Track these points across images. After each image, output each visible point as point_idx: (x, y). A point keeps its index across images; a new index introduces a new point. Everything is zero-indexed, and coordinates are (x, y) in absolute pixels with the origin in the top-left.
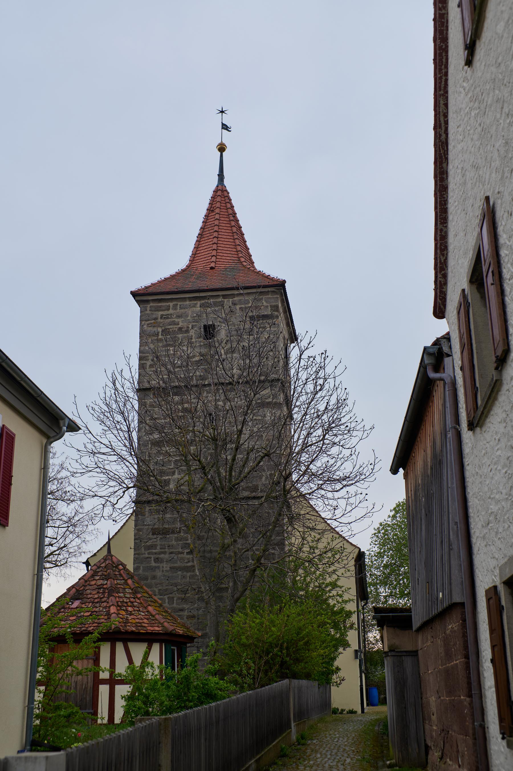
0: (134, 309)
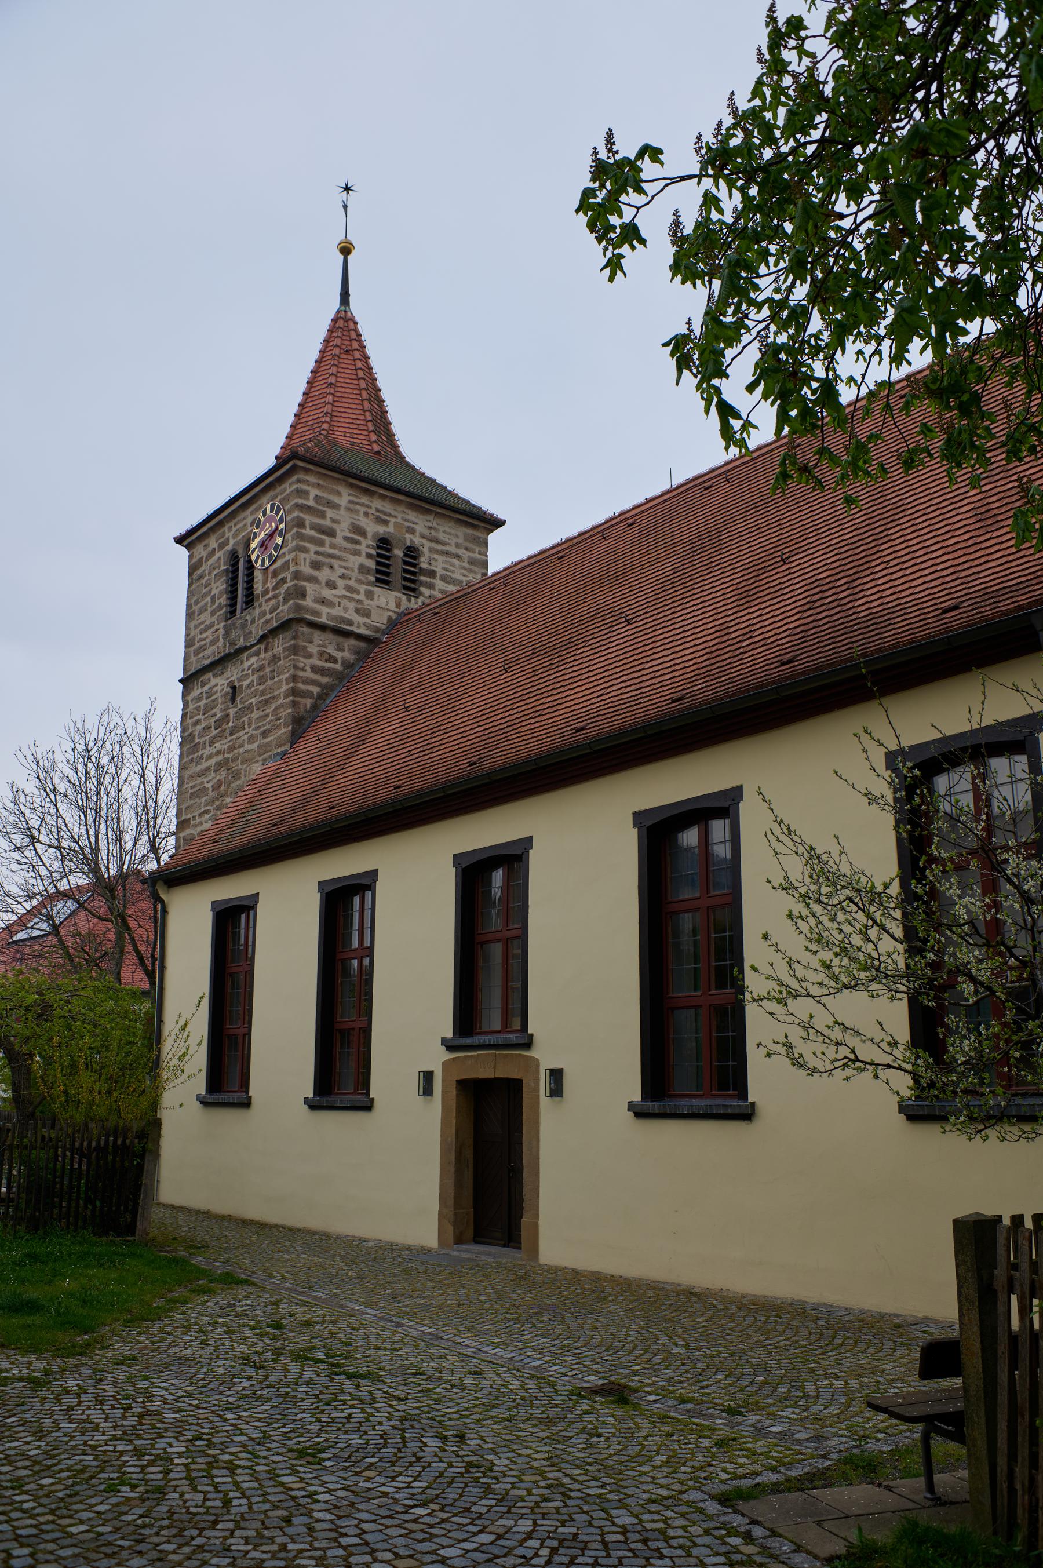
0: (181, 686)
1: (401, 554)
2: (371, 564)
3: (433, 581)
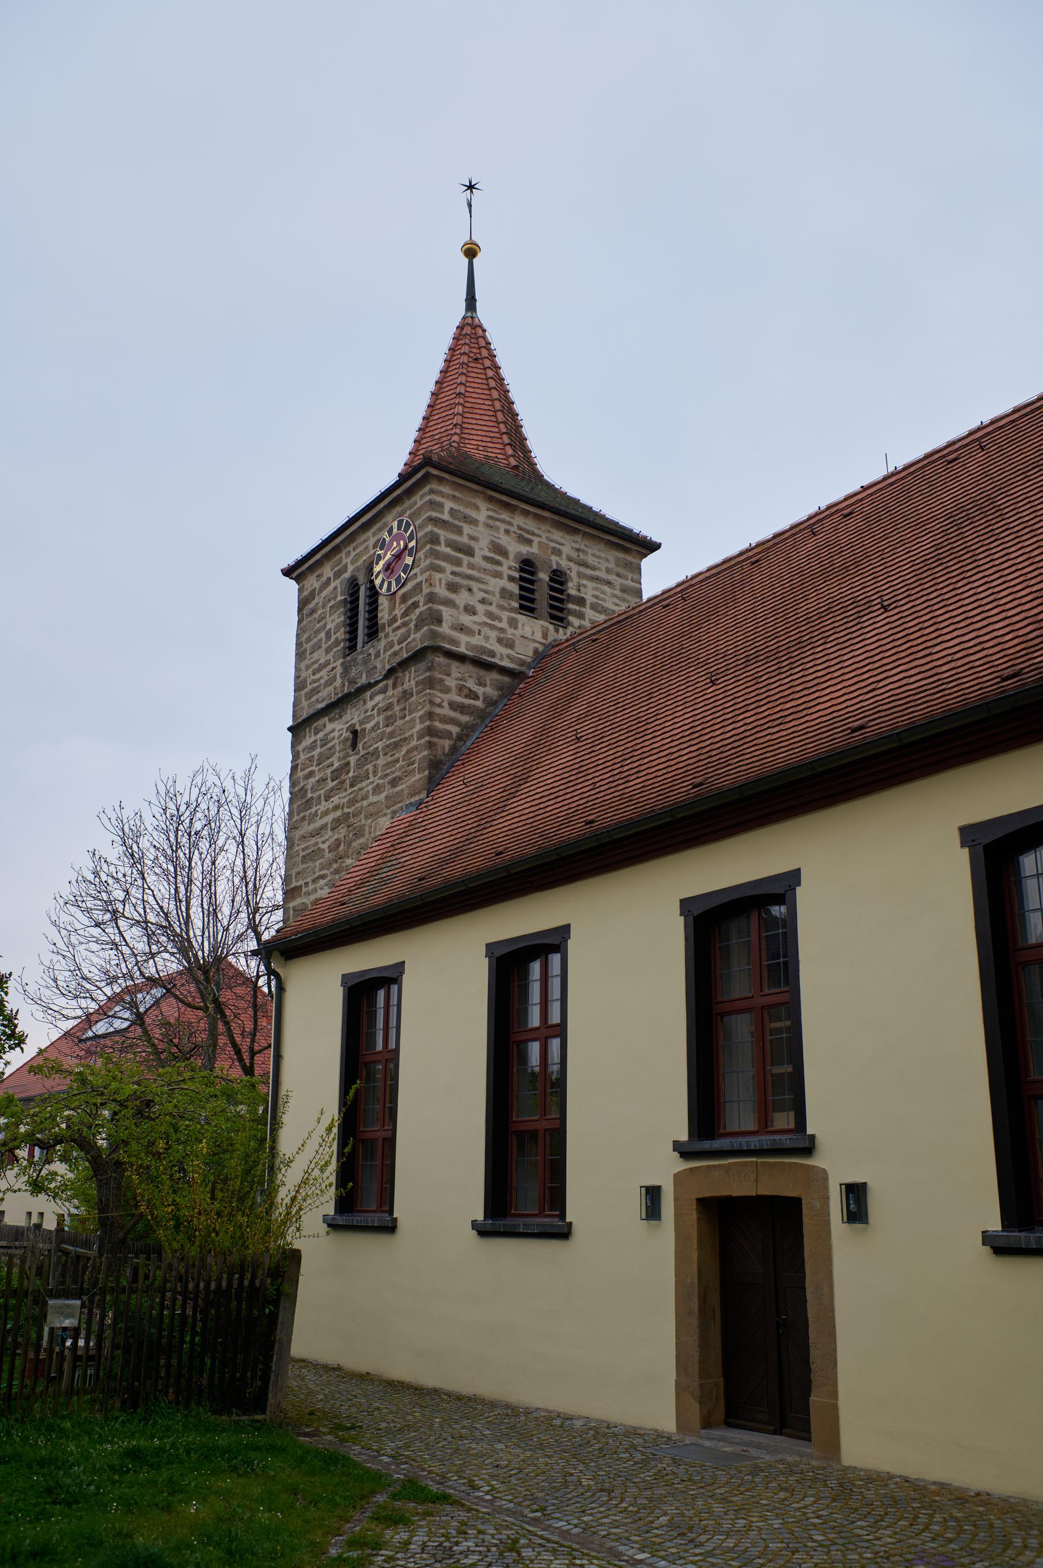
0: (290, 734)
1: (547, 579)
2: (514, 588)
3: (583, 609)
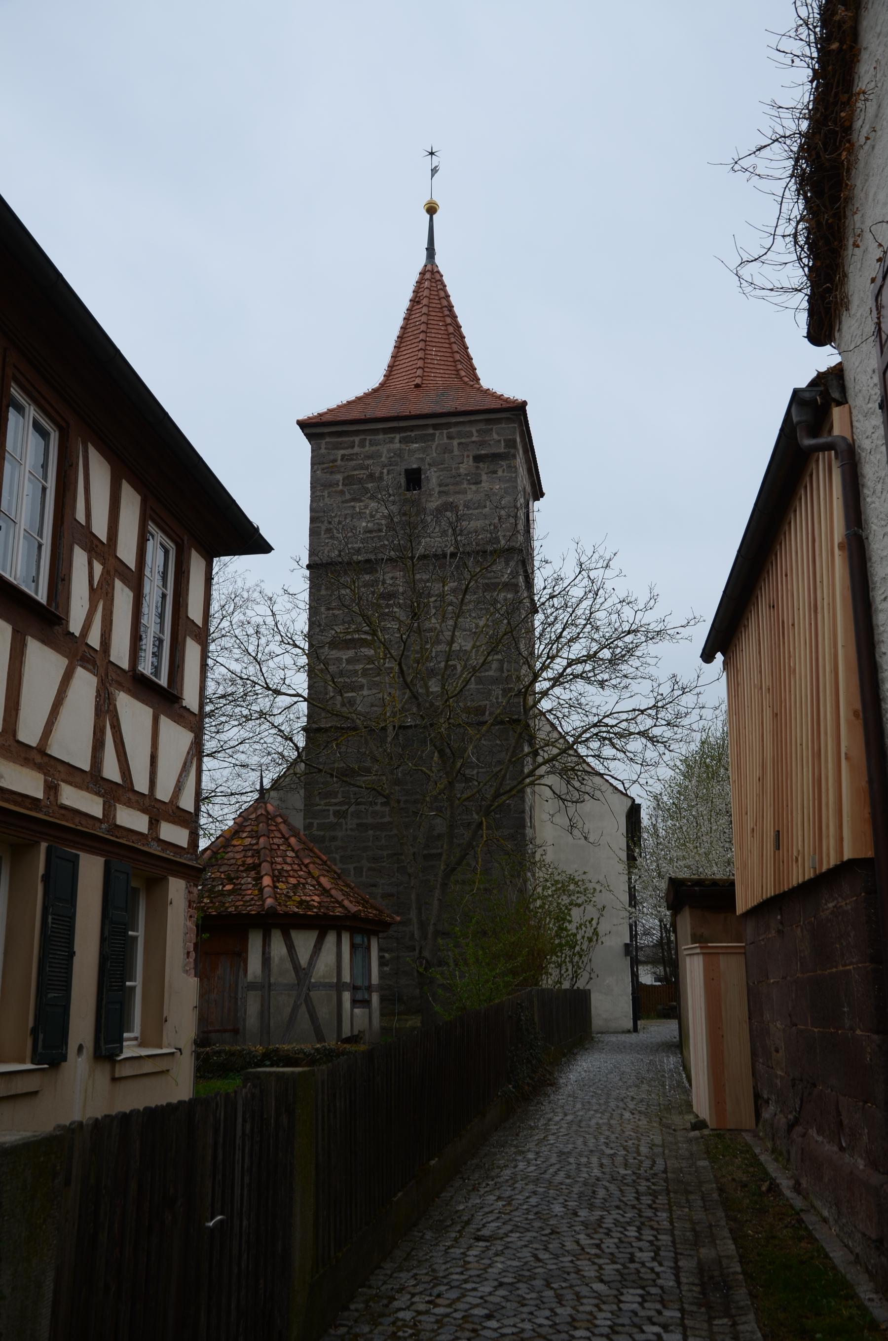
0: (303, 448)
